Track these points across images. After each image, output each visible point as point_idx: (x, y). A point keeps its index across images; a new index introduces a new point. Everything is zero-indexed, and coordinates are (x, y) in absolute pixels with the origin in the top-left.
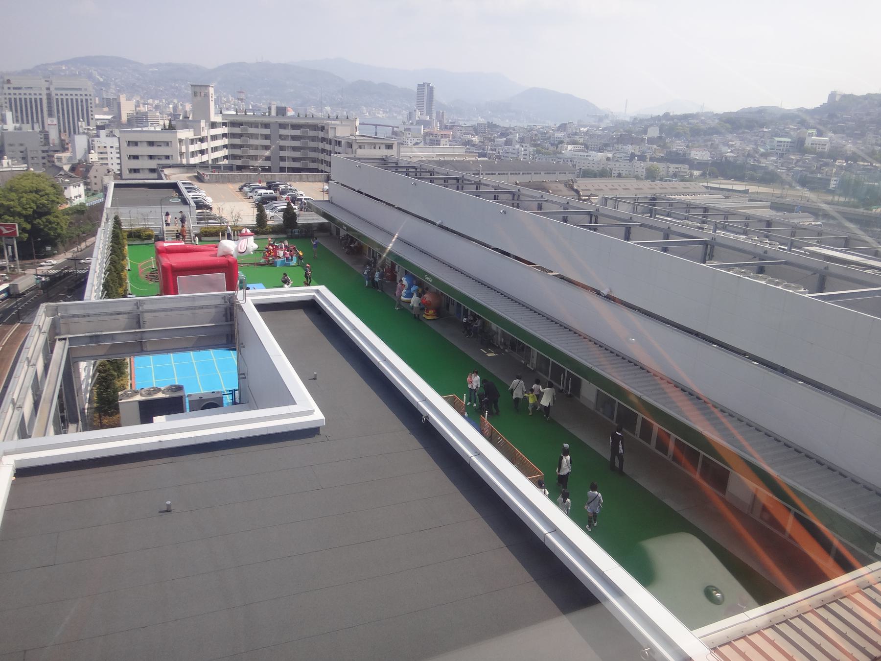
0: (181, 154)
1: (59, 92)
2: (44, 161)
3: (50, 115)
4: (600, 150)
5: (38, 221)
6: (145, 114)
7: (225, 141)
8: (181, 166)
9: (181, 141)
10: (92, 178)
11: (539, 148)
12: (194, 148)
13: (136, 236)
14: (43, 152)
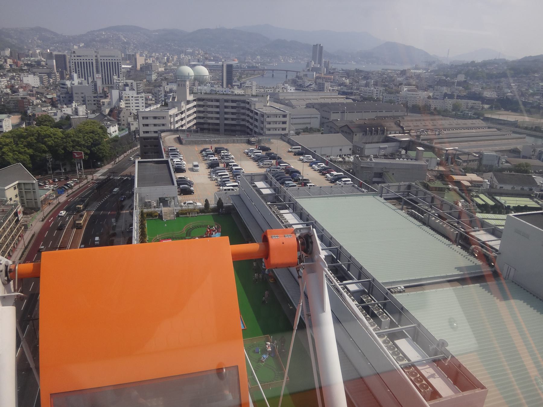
0: (171, 123)
1: (102, 58)
2: (95, 102)
3: (98, 72)
4: (425, 90)
5: (94, 148)
6: (150, 65)
7: (195, 109)
8: (170, 131)
9: (170, 116)
10: (122, 117)
11: (387, 88)
12: (179, 118)
13: (150, 215)
14: (94, 97)
